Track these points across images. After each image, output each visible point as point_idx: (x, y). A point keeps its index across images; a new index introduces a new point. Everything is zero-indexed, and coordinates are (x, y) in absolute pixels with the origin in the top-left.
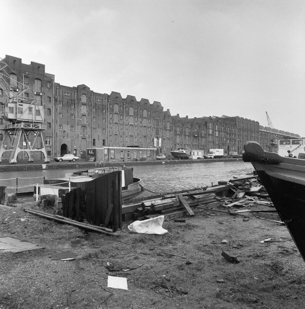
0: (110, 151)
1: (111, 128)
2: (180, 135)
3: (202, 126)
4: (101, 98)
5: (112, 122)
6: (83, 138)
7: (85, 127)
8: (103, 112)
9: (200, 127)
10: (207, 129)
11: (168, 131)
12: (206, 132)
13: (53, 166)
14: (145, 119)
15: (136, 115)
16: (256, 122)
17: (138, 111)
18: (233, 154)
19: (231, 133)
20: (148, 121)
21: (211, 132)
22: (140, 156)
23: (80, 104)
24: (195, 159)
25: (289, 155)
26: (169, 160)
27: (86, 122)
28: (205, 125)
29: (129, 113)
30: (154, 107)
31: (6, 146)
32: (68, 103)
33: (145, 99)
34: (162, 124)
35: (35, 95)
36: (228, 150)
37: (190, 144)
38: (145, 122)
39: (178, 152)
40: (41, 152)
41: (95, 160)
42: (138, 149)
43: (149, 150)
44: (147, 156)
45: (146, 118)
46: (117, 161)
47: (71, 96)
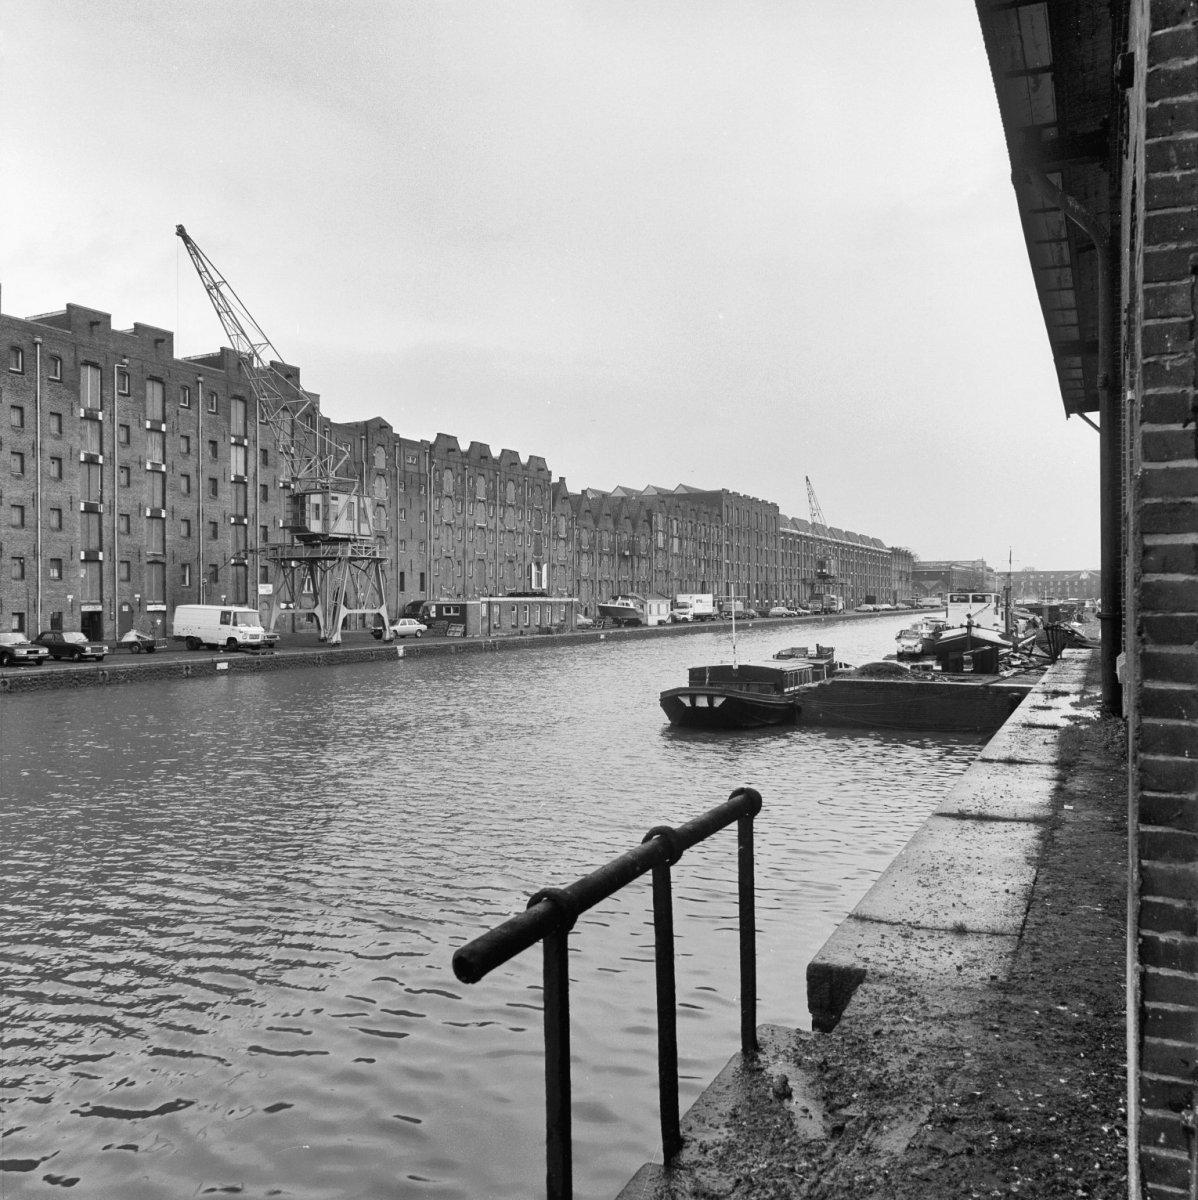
2: (590, 553)
3: (640, 522)
7: (383, 537)
9: (634, 526)
11: (562, 543)
14: (511, 508)
15: (492, 498)
23: (372, 475)
28: (609, 515)
35: (148, 430)
37: (613, 578)
38: (512, 520)
40: (379, 614)
41: (465, 634)
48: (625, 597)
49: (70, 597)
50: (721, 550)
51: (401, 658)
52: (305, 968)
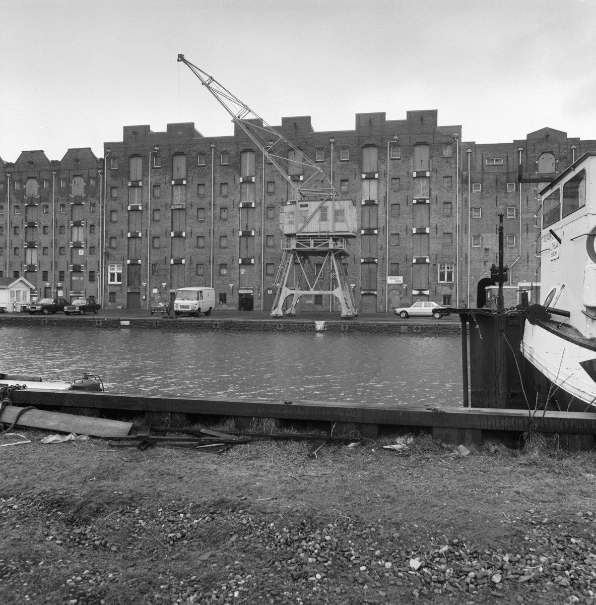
13: (340, 326)
31: (354, 285)
47: (508, 166)
49: (231, 285)
51: (318, 331)
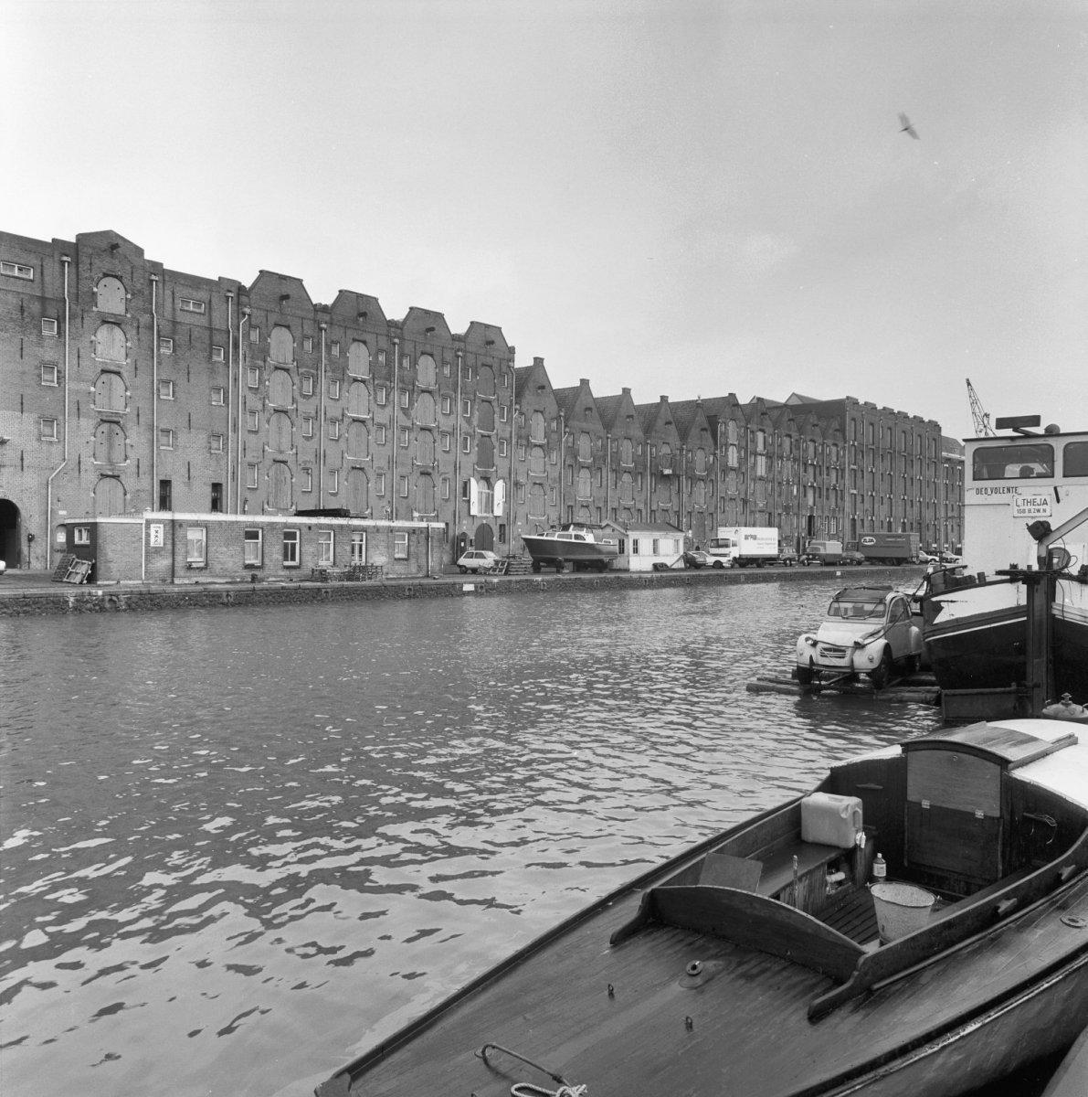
0: (179, 533)
1: (256, 432)
2: (595, 468)
3: (694, 431)
4: (203, 295)
5: (260, 407)
6: (104, 476)
7: (117, 423)
8: (215, 358)
9: (684, 435)
10: (716, 444)
11: (538, 452)
12: (711, 459)
15: (381, 377)
16: (930, 421)
17: (389, 362)
18: (822, 551)
19: (820, 463)
20: (438, 408)
21: (735, 460)
22: (357, 557)
24: (641, 572)
25: (1044, 554)
26: (506, 574)
27: (123, 400)
29: (344, 369)
30: (469, 348)
32: (26, 314)
33: (427, 312)
34: (510, 419)
36: (810, 533)
37: (641, 506)
38: (426, 411)
39: (555, 538)
41: (91, 578)
42: (341, 526)
43: (400, 529)
44: (391, 555)
45: (430, 392)
46: (225, 581)
48: (580, 526)
50: (843, 477)
52: (530, 845)
